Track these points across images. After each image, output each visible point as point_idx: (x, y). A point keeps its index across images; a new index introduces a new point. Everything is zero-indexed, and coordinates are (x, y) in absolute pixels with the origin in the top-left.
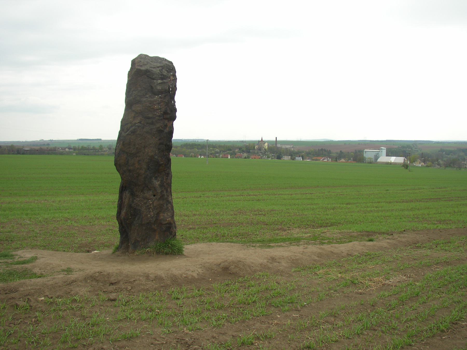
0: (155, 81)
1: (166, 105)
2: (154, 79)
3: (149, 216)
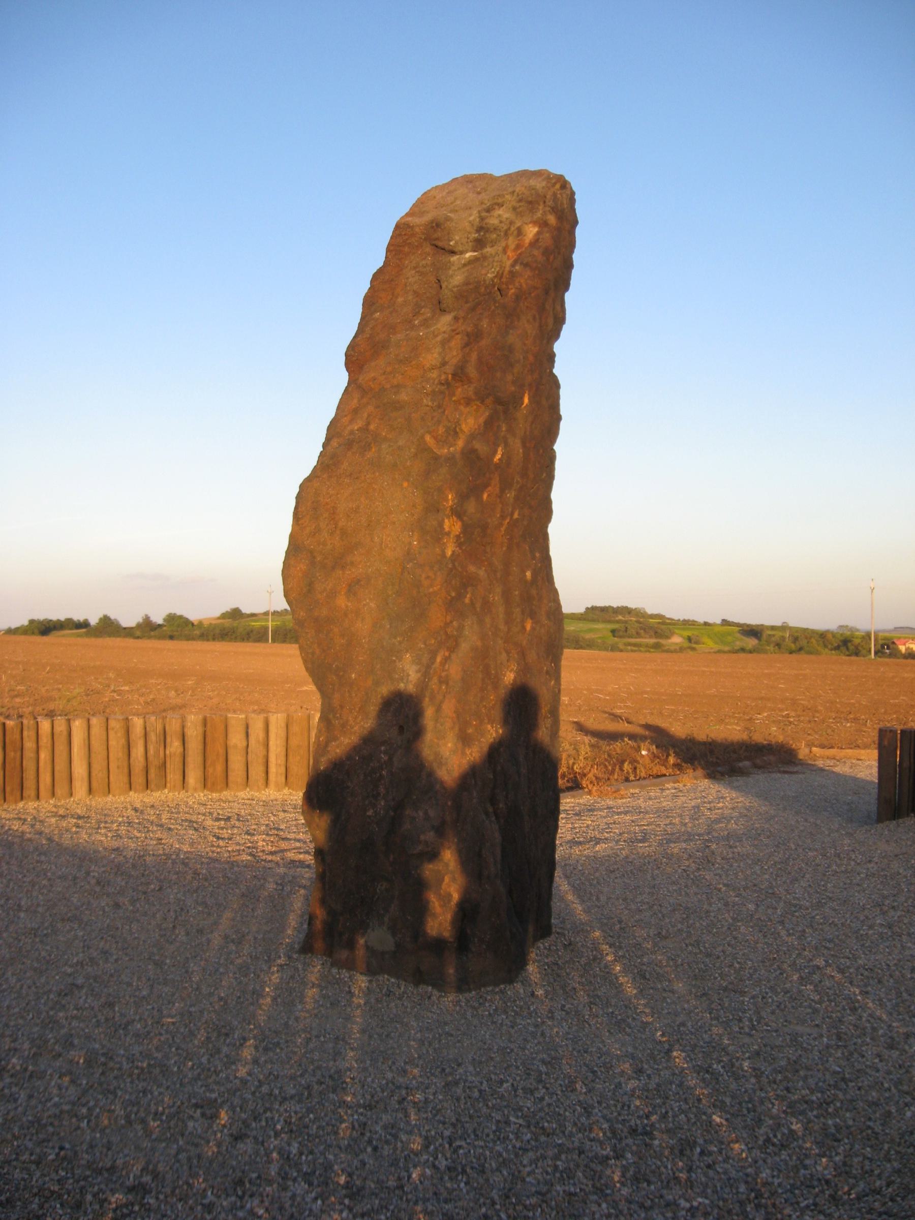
0: (454, 258)
1: (467, 345)
2: (453, 252)
3: (370, 813)
